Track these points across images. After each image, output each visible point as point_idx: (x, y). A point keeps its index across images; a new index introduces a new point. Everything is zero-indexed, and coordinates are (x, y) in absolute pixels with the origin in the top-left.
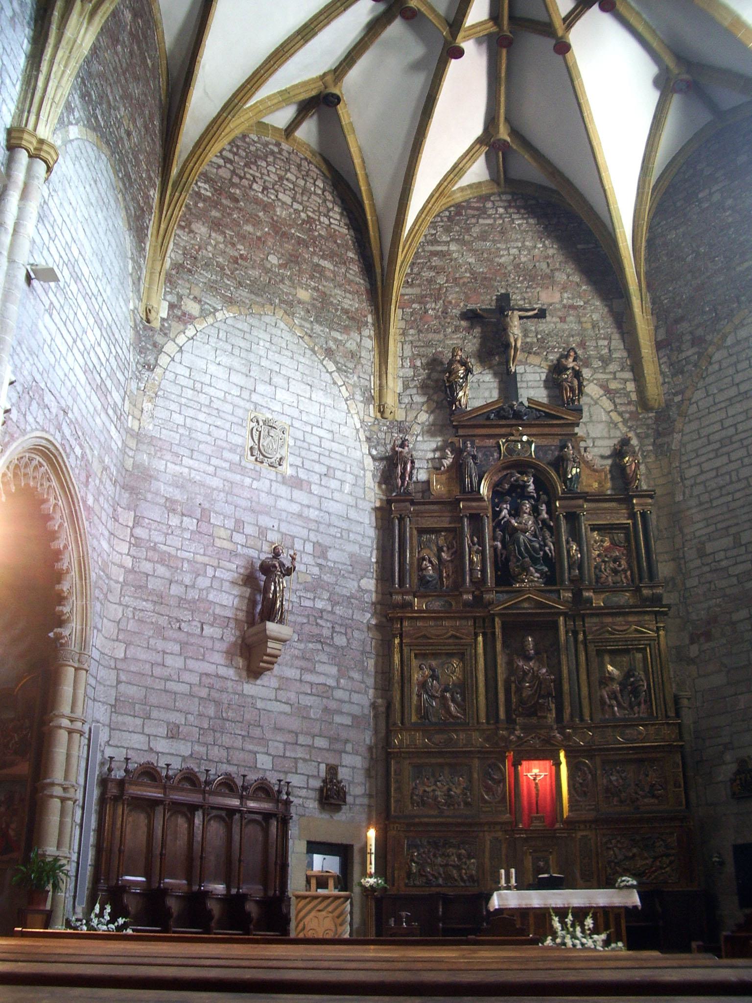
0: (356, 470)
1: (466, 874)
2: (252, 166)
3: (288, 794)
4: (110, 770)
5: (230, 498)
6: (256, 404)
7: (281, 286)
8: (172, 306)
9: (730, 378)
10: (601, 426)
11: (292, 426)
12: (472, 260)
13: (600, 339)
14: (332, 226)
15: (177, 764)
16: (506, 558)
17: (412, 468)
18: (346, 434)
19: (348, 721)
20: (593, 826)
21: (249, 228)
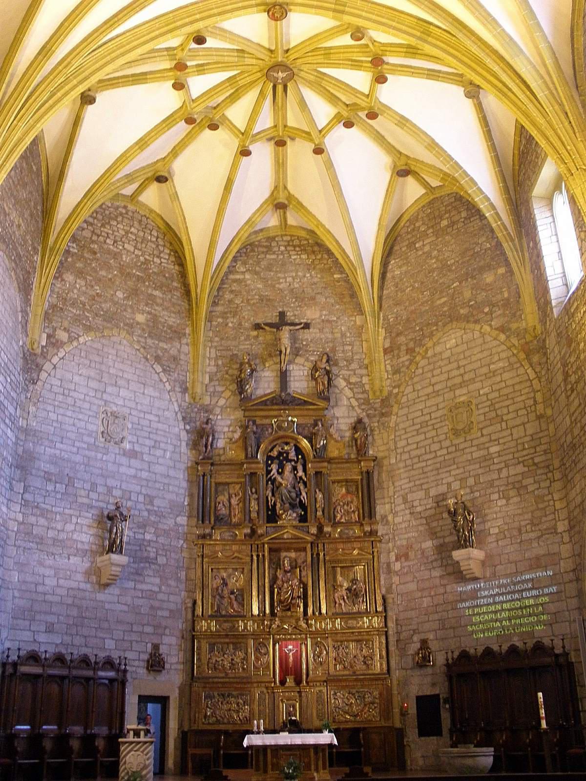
0: (175, 442)
2: (106, 226)
3: (125, 665)
4: (8, 656)
5: (87, 468)
6: (106, 401)
8: (49, 336)
9: (428, 380)
11: (130, 414)
12: (260, 286)
15: (52, 650)
18: (168, 416)
19: (166, 614)
21: (103, 273)
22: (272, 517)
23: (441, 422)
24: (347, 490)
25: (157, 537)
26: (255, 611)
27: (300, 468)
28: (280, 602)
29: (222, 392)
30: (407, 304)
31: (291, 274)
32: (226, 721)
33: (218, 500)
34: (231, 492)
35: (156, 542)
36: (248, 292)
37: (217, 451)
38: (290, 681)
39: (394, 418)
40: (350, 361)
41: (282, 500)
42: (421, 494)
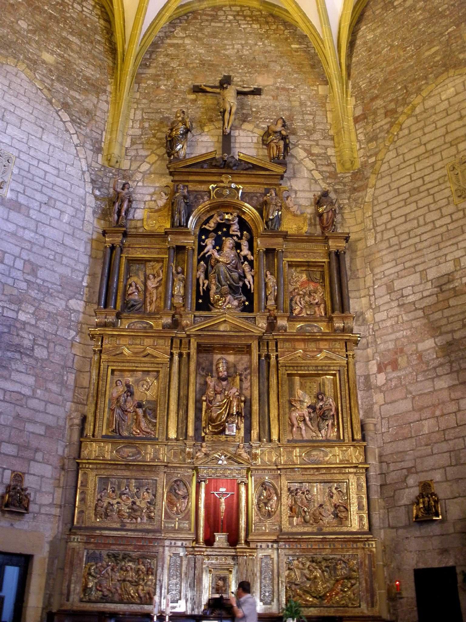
1: (143, 590)
7: (27, 46)
10: (303, 181)
11: (19, 157)
12: (202, 51)
13: (307, 114)
14: (84, 13)
16: (207, 287)
17: (129, 207)
19: (41, 430)
20: (275, 546)
22: (204, 303)
23: (440, 184)
24: (309, 276)
25: (37, 320)
26: (172, 435)
27: (245, 244)
28: (211, 420)
29: (147, 157)
30: (384, 64)
31: (240, 42)
32: (116, 597)
33: (130, 281)
34: (148, 272)
35: (35, 326)
36: (187, 56)
37: (133, 223)
38: (220, 538)
39: (370, 191)
40: (311, 132)
41: (219, 281)
42: (415, 278)
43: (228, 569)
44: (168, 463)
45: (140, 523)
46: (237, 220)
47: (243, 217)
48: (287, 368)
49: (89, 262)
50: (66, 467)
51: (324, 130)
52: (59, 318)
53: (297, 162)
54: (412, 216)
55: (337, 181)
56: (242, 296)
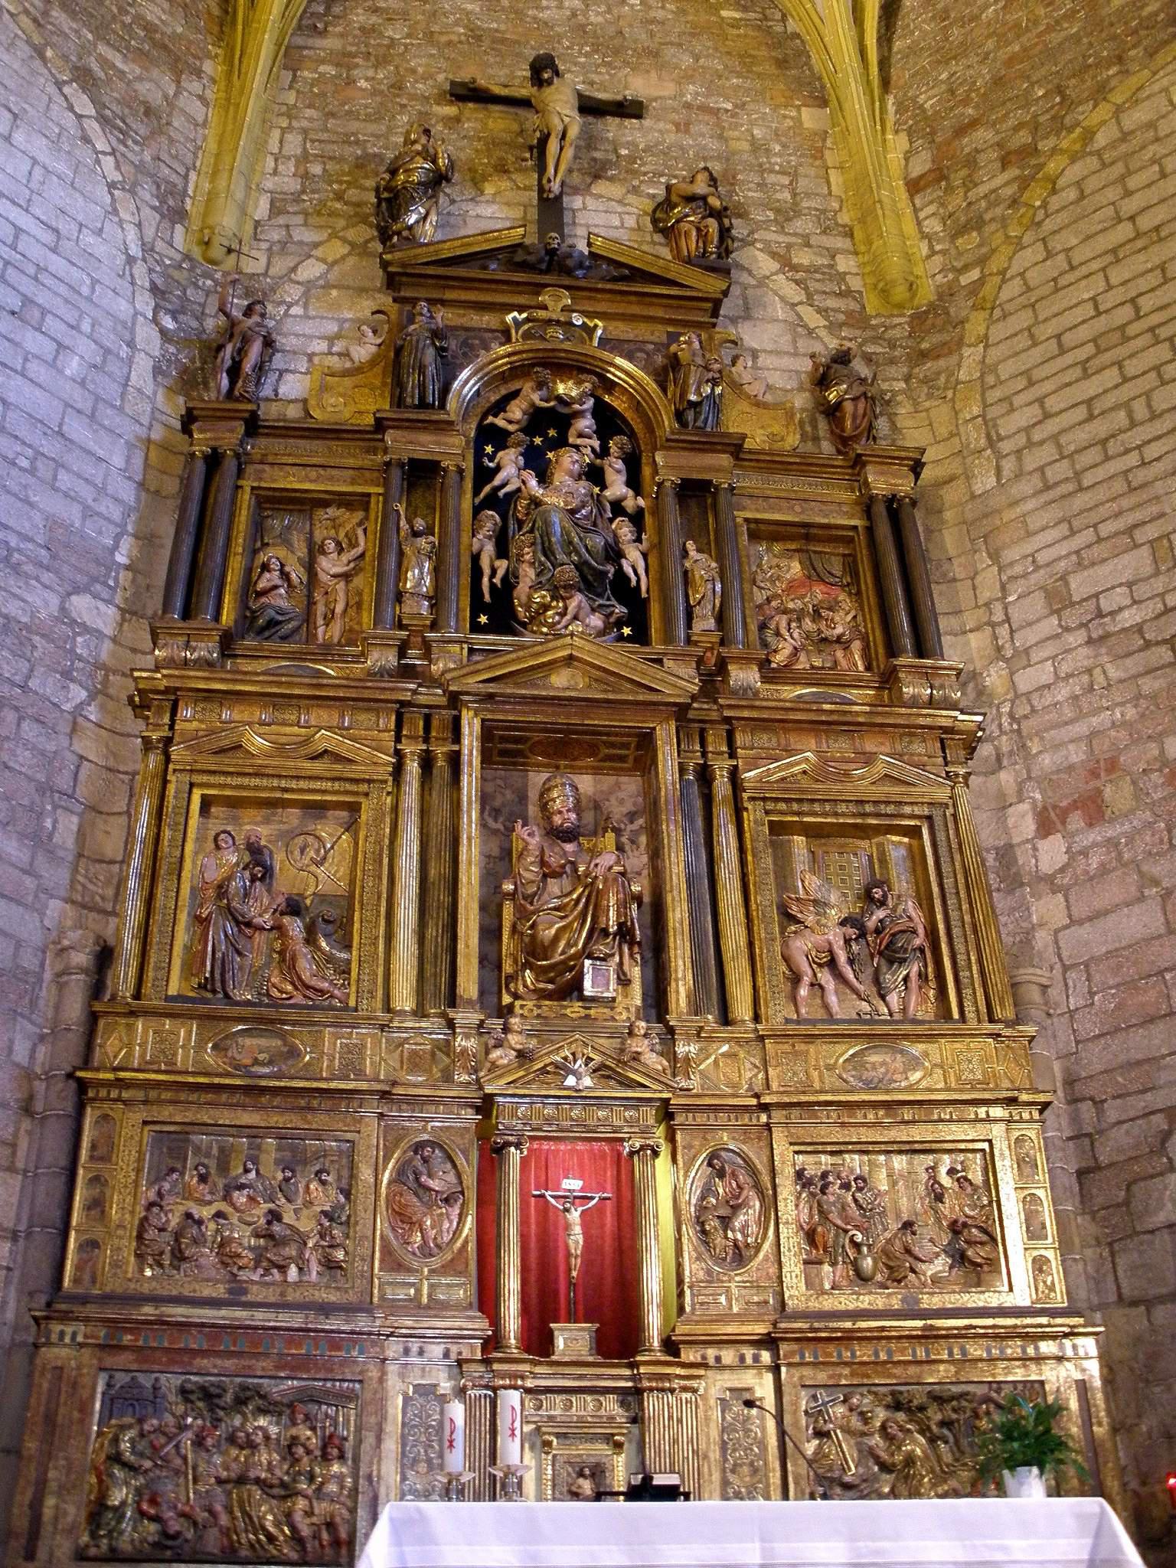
1: (309, 1513)
10: (774, 329)
13: (772, 171)
24: (810, 566)
29: (316, 245)
30: (990, 44)
33: (262, 557)
34: (318, 536)
38: (571, 1339)
39: (971, 355)
40: (785, 215)
43: (608, 1438)
44: (394, 1083)
45: (298, 1284)
46: (590, 403)
47: (607, 398)
48: (770, 806)
49: (138, 499)
50: (39, 1106)
51: (824, 211)
52: (36, 639)
53: (753, 282)
54: (1110, 400)
55: (869, 333)
56: (614, 602)
